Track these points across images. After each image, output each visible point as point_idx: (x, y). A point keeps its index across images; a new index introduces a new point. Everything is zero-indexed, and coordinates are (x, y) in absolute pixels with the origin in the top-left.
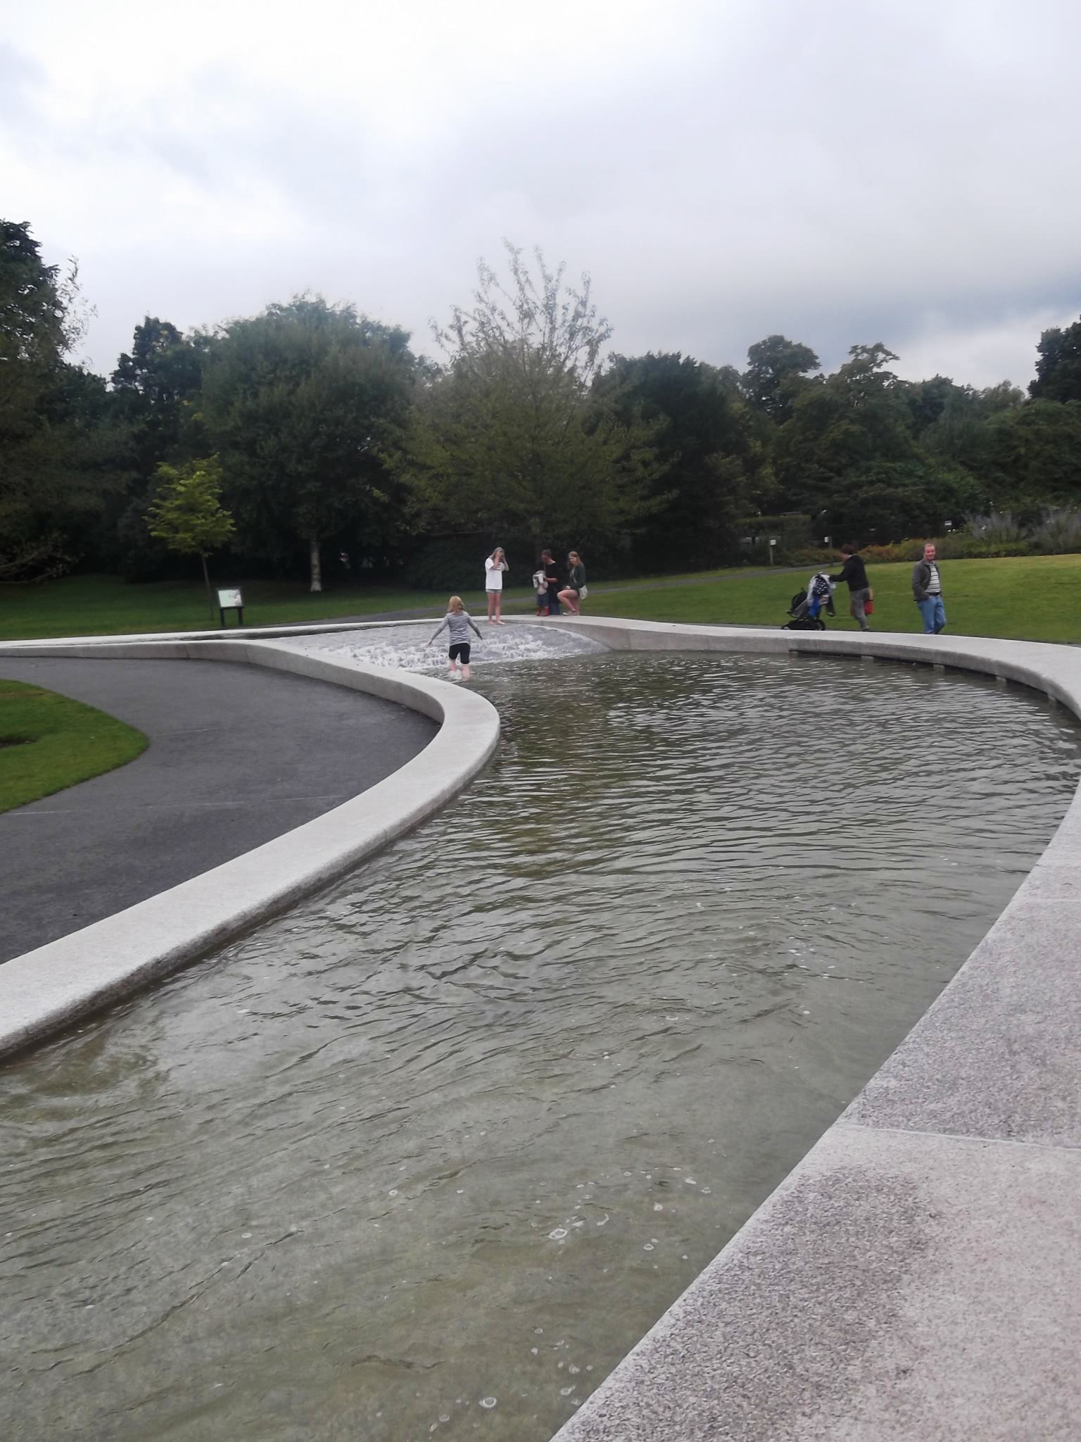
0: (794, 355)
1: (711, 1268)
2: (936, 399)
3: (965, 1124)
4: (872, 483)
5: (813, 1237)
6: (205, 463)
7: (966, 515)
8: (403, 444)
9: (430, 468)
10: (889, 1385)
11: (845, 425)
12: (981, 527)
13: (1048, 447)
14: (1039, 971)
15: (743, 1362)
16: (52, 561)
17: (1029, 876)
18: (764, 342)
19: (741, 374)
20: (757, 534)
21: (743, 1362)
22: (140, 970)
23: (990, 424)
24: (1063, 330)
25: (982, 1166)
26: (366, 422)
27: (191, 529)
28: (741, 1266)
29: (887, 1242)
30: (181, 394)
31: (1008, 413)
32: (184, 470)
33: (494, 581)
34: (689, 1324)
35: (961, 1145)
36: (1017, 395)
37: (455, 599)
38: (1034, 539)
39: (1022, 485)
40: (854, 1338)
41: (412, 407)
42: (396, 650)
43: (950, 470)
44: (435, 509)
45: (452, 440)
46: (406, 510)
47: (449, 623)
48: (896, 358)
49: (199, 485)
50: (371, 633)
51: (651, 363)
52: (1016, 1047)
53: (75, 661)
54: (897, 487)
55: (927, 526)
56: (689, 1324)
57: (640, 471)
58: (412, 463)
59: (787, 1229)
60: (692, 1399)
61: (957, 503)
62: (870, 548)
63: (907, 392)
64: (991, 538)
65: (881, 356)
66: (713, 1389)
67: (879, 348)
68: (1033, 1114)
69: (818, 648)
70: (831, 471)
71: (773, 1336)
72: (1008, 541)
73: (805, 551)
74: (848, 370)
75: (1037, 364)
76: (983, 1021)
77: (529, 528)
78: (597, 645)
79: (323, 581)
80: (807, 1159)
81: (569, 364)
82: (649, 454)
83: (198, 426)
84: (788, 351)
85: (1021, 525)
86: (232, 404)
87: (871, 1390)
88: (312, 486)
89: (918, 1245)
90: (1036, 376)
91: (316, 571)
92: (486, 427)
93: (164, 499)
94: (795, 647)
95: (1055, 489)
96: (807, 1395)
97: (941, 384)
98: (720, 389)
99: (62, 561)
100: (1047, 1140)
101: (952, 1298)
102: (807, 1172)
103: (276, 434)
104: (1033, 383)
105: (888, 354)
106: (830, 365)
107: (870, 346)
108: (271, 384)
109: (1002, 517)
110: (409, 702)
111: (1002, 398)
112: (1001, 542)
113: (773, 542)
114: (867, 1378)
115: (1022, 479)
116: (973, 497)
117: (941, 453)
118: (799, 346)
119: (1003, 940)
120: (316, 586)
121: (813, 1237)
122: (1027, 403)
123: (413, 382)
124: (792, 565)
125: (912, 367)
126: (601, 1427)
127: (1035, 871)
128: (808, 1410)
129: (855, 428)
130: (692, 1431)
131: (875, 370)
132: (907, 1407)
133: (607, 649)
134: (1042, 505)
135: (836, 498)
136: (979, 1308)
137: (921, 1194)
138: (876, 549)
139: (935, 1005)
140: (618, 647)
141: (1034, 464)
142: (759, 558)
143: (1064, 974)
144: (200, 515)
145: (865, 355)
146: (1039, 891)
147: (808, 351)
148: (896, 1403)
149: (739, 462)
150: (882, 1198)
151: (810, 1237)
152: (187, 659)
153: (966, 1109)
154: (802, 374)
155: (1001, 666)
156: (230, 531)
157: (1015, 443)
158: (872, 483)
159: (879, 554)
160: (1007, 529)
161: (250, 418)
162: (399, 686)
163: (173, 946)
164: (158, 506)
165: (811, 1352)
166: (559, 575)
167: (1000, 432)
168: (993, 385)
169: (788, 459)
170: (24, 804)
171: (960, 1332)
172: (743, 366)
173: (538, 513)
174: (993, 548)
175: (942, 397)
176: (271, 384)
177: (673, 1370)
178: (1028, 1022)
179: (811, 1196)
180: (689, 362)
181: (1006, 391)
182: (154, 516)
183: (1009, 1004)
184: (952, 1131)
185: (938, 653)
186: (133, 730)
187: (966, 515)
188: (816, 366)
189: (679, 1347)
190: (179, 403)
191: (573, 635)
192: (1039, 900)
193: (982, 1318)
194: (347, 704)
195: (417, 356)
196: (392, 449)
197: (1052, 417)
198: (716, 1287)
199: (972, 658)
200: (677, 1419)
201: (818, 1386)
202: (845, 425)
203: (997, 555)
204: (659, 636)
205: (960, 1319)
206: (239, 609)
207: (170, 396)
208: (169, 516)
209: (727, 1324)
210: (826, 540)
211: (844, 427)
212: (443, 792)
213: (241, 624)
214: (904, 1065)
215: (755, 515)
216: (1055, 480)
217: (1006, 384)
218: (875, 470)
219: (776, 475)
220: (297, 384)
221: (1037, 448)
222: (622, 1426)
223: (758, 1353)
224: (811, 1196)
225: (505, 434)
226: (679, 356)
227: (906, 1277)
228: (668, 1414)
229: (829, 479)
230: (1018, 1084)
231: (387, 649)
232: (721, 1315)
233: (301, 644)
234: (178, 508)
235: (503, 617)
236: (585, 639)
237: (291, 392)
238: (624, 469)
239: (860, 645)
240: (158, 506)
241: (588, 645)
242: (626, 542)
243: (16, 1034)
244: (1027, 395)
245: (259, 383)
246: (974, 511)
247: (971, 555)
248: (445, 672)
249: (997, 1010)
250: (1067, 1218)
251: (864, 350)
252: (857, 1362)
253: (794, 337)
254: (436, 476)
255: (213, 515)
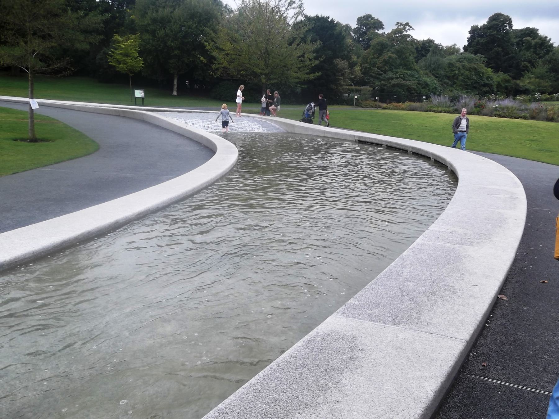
0: (374, 23)
1: (276, 361)
2: (427, 48)
3: (380, 319)
4: (397, 78)
5: (316, 353)
6: (134, 36)
7: (432, 95)
8: (215, 40)
9: (225, 51)
10: (331, 406)
11: (390, 54)
12: (436, 100)
13: (467, 72)
14: (419, 267)
15: (281, 394)
16: (66, 69)
17: (424, 233)
18: (364, 16)
19: (353, 28)
20: (350, 93)
21: (281, 394)
22: (82, 234)
23: (446, 60)
24: (479, 26)
25: (382, 334)
26: (201, 29)
27: (126, 63)
28: (287, 361)
29: (348, 353)
30: (127, 7)
31: (453, 57)
32: (125, 38)
33: (239, 100)
34: (264, 379)
35: (376, 326)
36: (458, 50)
37: (224, 105)
38: (455, 107)
39: (455, 86)
40: (322, 389)
41: (220, 25)
42: (203, 122)
43: (428, 76)
44: (224, 68)
45: (234, 40)
46: (213, 67)
47: (222, 113)
48: (413, 29)
49: (131, 46)
50: (194, 114)
51: (317, 19)
52: (404, 294)
53: (73, 111)
54: (407, 81)
55: (416, 98)
56: (264, 379)
57: (308, 62)
58: (217, 48)
59: (307, 350)
60: (260, 405)
61: (429, 90)
62: (393, 103)
63: (416, 43)
64: (440, 104)
65: (407, 27)
66: (268, 402)
67: (407, 24)
68: (405, 318)
69: (366, 140)
70: (382, 71)
71: (294, 386)
72: (446, 107)
73: (368, 102)
74: (394, 32)
75: (468, 38)
76: (395, 283)
77: (261, 80)
78: (282, 129)
79: (177, 91)
80: (319, 326)
81: (285, 15)
82: (312, 56)
83: (133, 21)
84: (372, 21)
85: (452, 101)
86: (147, 13)
87: (325, 407)
88: (176, 52)
89: (353, 359)
90: (466, 44)
91: (175, 87)
92: (249, 37)
93: (116, 50)
94: (357, 139)
95: (467, 89)
96: (301, 407)
97: (430, 42)
98: (344, 33)
99: (70, 69)
100: (407, 327)
101: (361, 378)
102: (318, 331)
103: (164, 29)
104: (465, 46)
105: (410, 27)
106: (388, 29)
107: (404, 23)
108: (164, 7)
109: (445, 98)
110: (205, 143)
111: (452, 50)
112: (443, 107)
113: (356, 97)
114: (324, 403)
115: (455, 84)
116: (435, 88)
117: (426, 69)
118: (377, 19)
119: (408, 255)
120: (175, 93)
121: (316, 353)
122: (462, 54)
123: (222, 14)
124: (362, 107)
125: (419, 33)
126: (225, 412)
127: (427, 231)
128: (300, 412)
129: (394, 56)
130: (258, 416)
131: (404, 33)
132: (336, 414)
133: (285, 131)
134: (460, 94)
135: (383, 82)
136: (369, 382)
137: (358, 342)
138: (395, 104)
139: (379, 276)
140: (290, 131)
141: (461, 78)
142: (350, 102)
143: (428, 269)
144: (130, 58)
145: (402, 27)
146: (426, 239)
147: (380, 22)
148: (333, 412)
149: (347, 63)
150: (344, 342)
151: (314, 353)
152: (119, 116)
153: (381, 314)
154: (376, 31)
155: (433, 154)
156: (142, 67)
157: (454, 69)
158: (397, 78)
159: (396, 106)
160: (446, 103)
161: (154, 21)
162: (202, 137)
163: (96, 226)
164: (113, 52)
165: (306, 392)
166: (271, 100)
167: (450, 64)
168: (450, 45)
169: (366, 65)
170: (46, 166)
171: (361, 390)
172: (354, 25)
173: (265, 74)
174: (440, 109)
175: (430, 47)
176: (164, 7)
177: (255, 395)
178: (411, 285)
179: (318, 339)
180: (332, 21)
181: (454, 48)
182: (111, 56)
183: (406, 278)
184: (374, 321)
185: (410, 147)
186: (94, 142)
187: (432, 95)
188: (383, 28)
189: (259, 387)
190: (126, 10)
191: (273, 124)
192: (425, 242)
193: (369, 386)
194: (181, 141)
195: (225, 4)
196: (210, 41)
197: (470, 60)
198: (277, 368)
199: (423, 150)
200: (253, 411)
201: (306, 404)
202: (390, 54)
203: (441, 112)
204: (306, 128)
205: (362, 385)
206: (143, 98)
207: (122, 7)
208: (117, 57)
209: (278, 381)
210: (377, 98)
211: (389, 55)
212: (211, 179)
213: (143, 105)
214: (362, 296)
215: (351, 85)
216: (467, 85)
217: (455, 45)
218: (399, 73)
219: (361, 70)
220: (175, 9)
221: (462, 72)
222: (232, 412)
223: (287, 391)
224: (318, 339)
225: (256, 41)
226: (329, 18)
227: (346, 370)
228: (250, 409)
229: (381, 75)
230: (402, 307)
231: (199, 121)
232: (276, 377)
233: (165, 115)
234: (121, 54)
235: (241, 114)
236: (277, 126)
237: (172, 12)
238: (301, 61)
239: (382, 141)
240: (113, 52)
241: (278, 129)
242: (299, 90)
243: (29, 253)
244: (462, 51)
245: (159, 6)
246: (435, 94)
247: (431, 111)
248: (220, 132)
249: (401, 280)
250: (408, 354)
251: (401, 24)
252: (322, 397)
253: (375, 16)
254: (226, 54)
255: (135, 59)
